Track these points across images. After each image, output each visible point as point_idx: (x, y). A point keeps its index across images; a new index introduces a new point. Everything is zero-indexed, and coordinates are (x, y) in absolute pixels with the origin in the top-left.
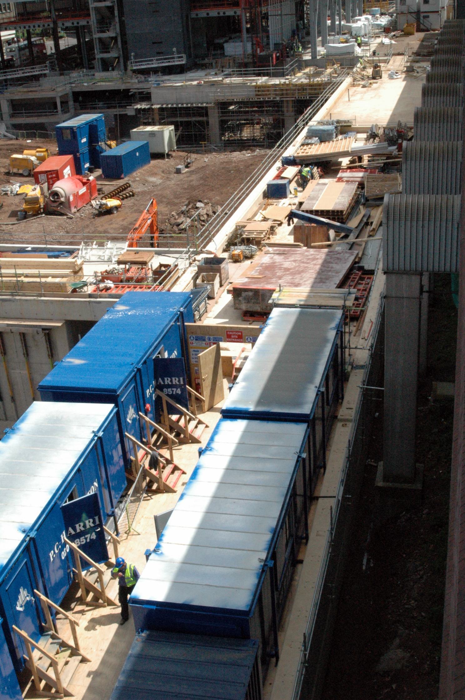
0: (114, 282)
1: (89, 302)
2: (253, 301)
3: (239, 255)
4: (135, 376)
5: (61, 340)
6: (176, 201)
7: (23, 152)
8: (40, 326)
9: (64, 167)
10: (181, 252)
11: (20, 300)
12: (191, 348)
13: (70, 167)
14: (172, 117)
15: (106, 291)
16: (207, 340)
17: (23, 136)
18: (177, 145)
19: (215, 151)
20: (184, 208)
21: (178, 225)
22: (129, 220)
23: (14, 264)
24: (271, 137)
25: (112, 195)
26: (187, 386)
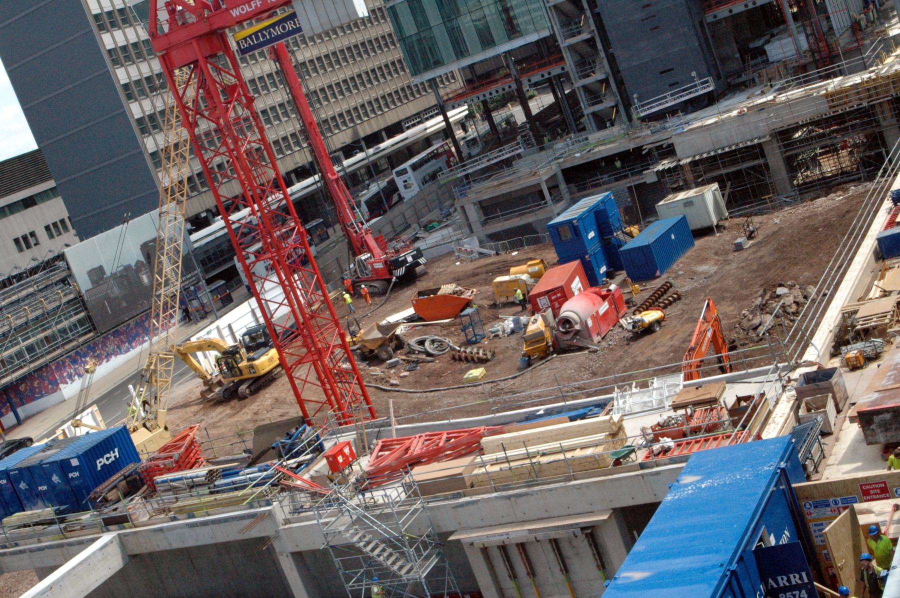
0: (673, 439)
1: (642, 476)
2: (894, 427)
3: (856, 357)
4: (729, 583)
5: (612, 540)
6: (745, 292)
7: (509, 271)
8: (577, 524)
9: (571, 280)
10: (765, 373)
11: (540, 491)
12: (810, 521)
13: (581, 281)
14: (711, 170)
15: (664, 454)
16: (832, 505)
17: (505, 249)
18: (728, 209)
19: (788, 204)
20: (759, 301)
21: (755, 328)
22: (681, 336)
23: (522, 440)
24: (868, 162)
25: (648, 306)
26: (815, 583)
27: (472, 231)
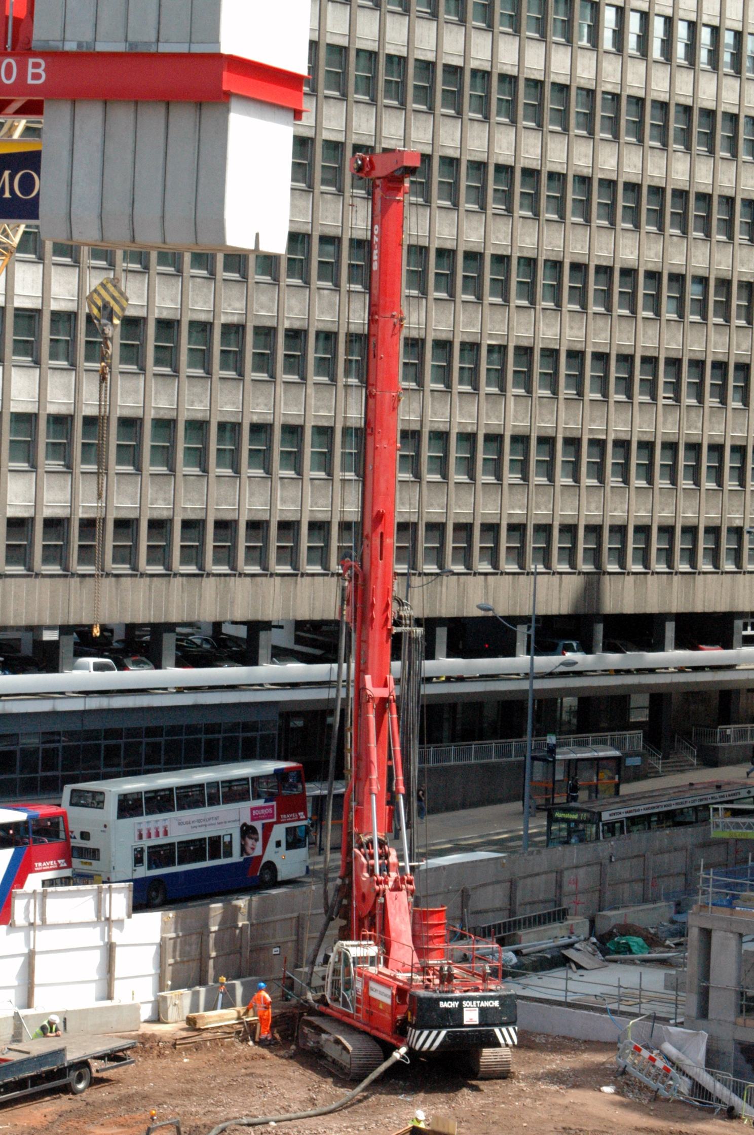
27: (704, 1013)
